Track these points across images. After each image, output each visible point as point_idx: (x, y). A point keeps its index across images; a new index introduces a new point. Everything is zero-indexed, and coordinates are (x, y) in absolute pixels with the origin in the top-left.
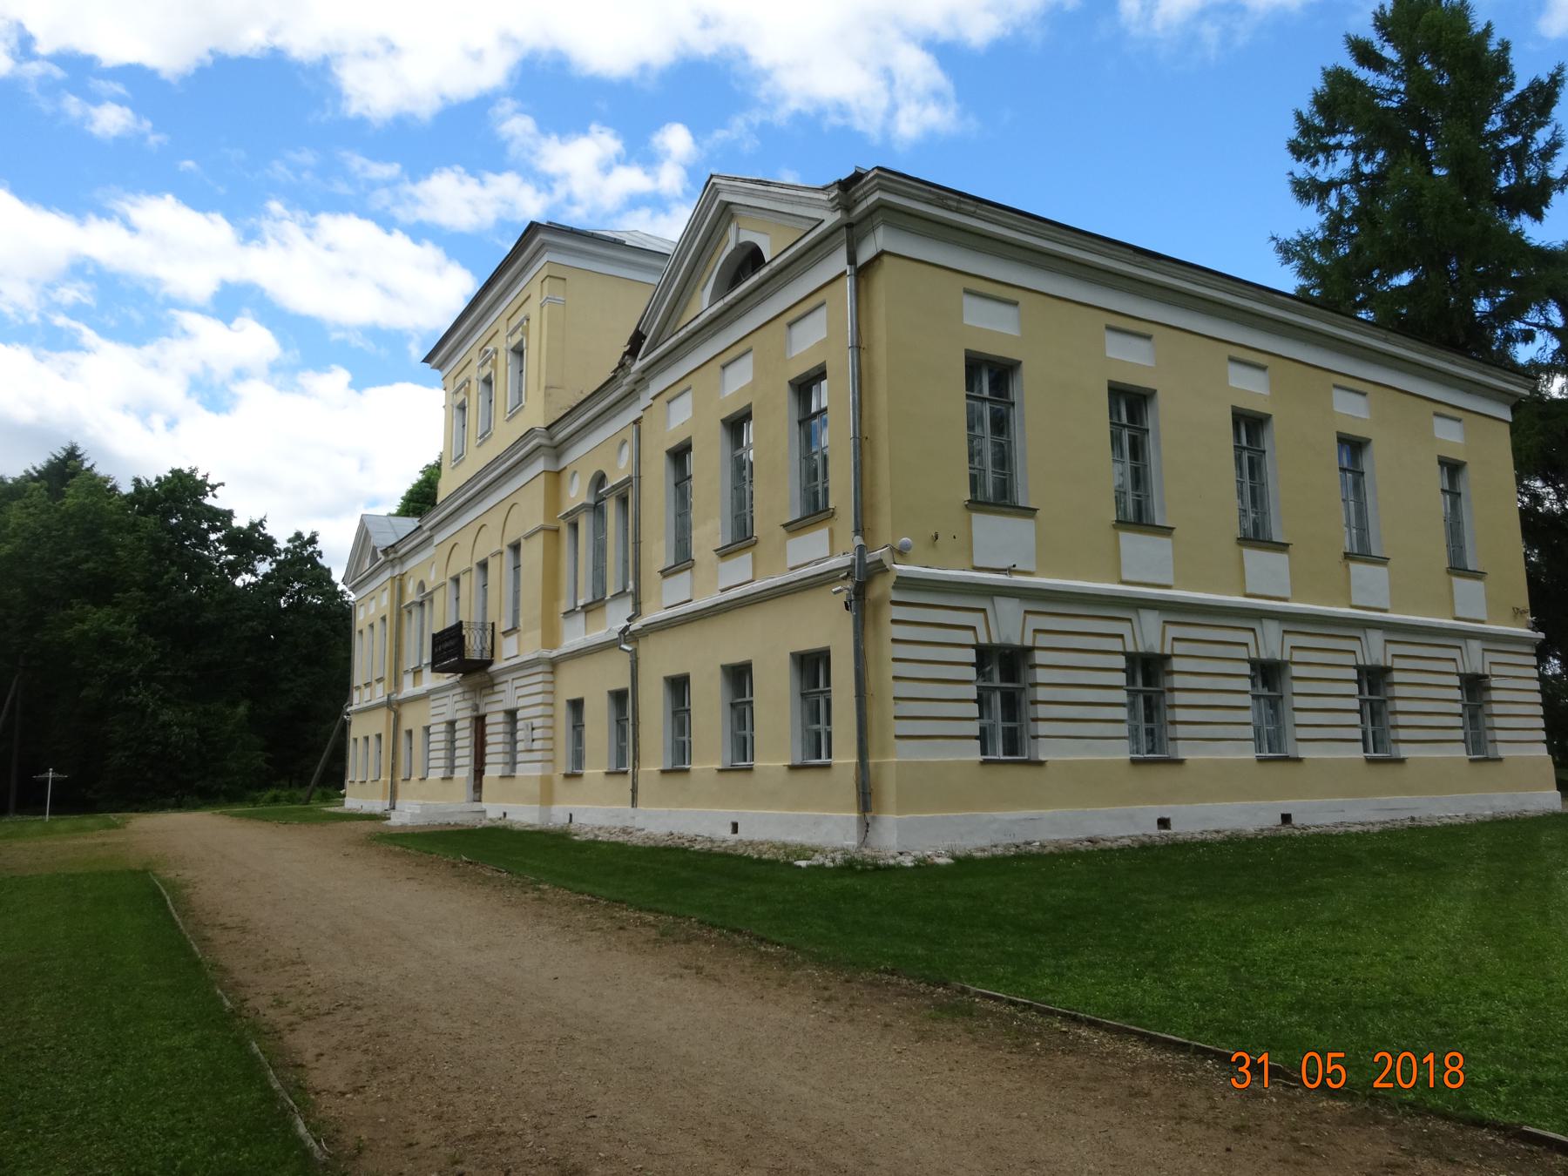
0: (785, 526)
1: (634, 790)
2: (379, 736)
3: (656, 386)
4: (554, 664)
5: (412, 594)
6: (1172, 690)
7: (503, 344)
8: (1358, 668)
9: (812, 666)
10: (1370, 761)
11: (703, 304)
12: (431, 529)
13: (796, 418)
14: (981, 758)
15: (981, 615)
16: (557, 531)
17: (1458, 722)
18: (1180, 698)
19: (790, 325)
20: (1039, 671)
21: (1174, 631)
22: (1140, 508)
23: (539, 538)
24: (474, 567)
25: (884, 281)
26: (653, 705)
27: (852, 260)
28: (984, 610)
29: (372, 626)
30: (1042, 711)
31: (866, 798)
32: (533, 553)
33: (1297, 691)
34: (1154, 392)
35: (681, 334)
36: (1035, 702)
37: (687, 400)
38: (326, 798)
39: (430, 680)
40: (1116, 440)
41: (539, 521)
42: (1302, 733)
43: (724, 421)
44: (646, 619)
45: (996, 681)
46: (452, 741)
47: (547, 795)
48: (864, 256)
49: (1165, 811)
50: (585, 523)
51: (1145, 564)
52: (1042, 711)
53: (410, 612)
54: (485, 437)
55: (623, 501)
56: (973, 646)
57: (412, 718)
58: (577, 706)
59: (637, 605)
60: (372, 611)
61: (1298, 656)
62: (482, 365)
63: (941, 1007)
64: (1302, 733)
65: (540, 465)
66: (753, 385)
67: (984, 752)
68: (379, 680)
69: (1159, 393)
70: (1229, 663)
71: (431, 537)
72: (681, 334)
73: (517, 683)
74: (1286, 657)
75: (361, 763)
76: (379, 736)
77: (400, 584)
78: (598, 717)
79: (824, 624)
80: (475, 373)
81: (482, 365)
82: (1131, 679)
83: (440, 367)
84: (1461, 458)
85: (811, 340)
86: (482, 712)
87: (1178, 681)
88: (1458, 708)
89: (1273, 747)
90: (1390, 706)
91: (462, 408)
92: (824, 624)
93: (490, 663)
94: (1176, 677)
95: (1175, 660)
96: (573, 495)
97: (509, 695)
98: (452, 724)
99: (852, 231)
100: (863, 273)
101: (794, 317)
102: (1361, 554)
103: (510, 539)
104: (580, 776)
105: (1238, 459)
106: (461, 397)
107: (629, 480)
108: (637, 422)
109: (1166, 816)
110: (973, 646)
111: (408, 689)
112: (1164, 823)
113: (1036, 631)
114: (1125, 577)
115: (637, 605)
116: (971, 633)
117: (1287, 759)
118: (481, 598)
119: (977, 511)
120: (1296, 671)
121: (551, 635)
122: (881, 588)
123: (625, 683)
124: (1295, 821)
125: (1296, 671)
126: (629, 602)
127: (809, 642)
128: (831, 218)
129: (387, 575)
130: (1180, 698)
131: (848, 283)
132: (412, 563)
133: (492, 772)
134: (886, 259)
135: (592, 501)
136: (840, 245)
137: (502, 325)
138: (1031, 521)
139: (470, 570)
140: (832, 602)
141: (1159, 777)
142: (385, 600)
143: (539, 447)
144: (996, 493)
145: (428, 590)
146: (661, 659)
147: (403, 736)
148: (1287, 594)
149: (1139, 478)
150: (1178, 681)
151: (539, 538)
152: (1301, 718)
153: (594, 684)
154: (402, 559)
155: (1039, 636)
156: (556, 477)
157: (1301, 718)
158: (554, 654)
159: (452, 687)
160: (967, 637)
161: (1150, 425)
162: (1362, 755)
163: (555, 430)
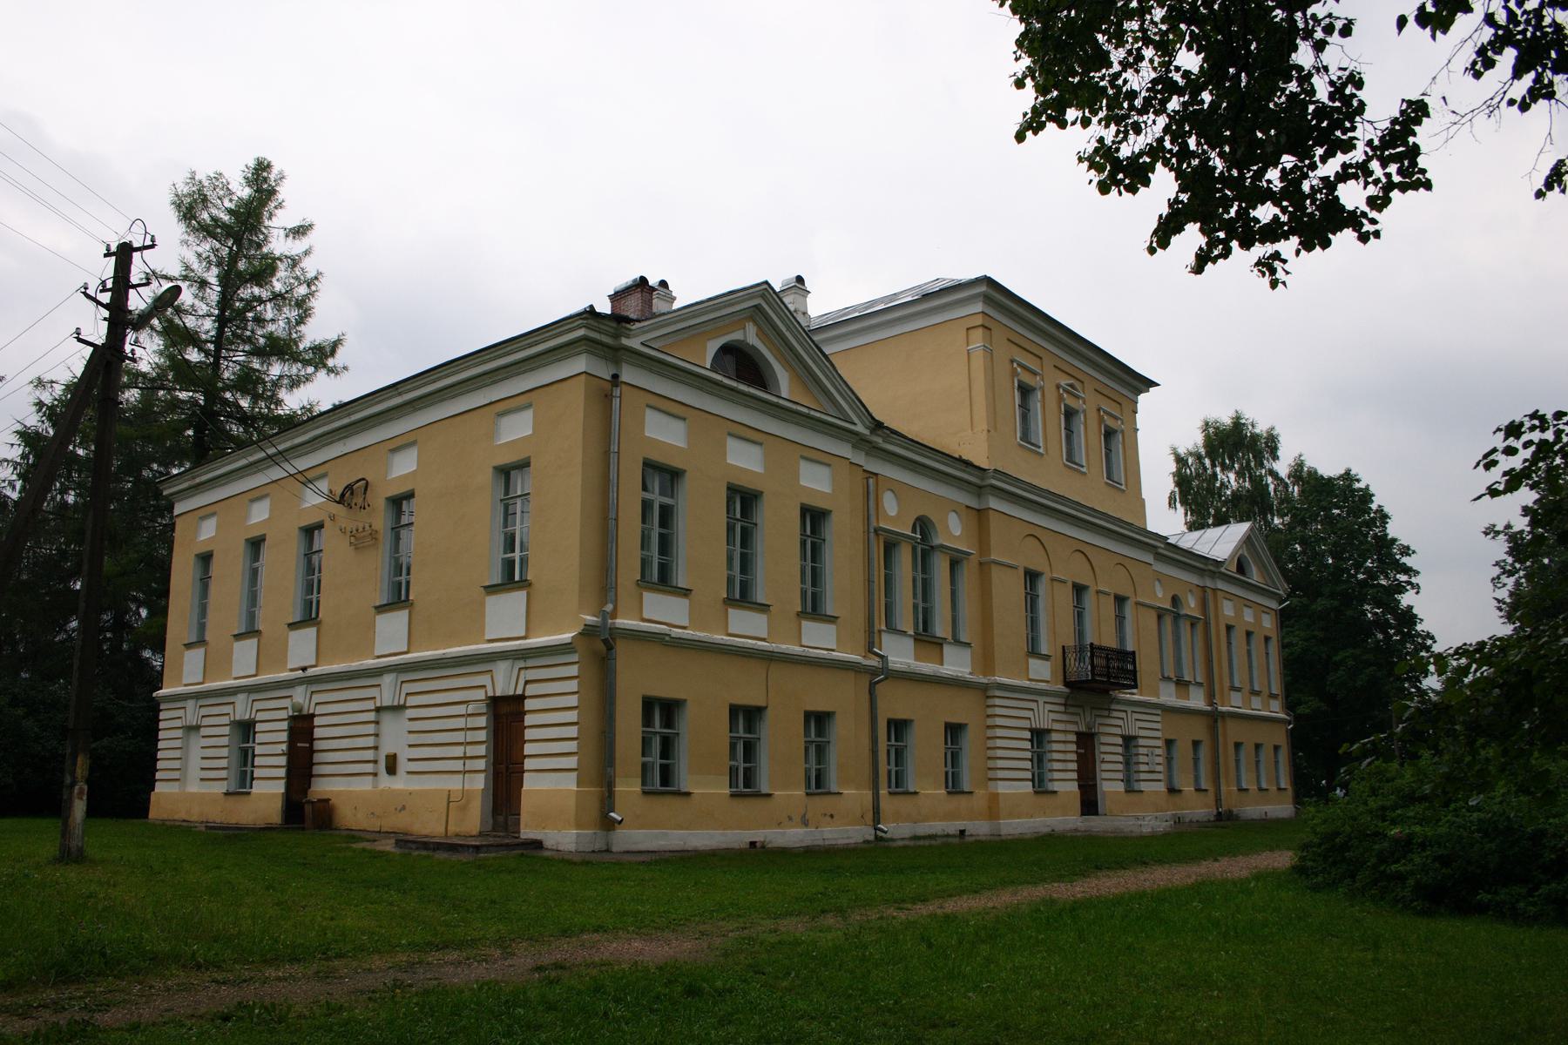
8: (1031, 730)
17: (1120, 767)
22: (746, 588)
34: (684, 471)
40: (730, 529)
45: (741, 733)
63: (1337, 834)
67: (644, 784)
69: (765, 498)
84: (677, 463)
88: (1028, 755)
89: (745, 783)
90: (1049, 756)
95: (527, 701)
105: (803, 543)
117: (907, 793)
118: (866, 705)
119: (733, 606)
133: (628, 788)
138: (833, 627)
149: (746, 564)
160: (1026, 724)
161: (759, 521)
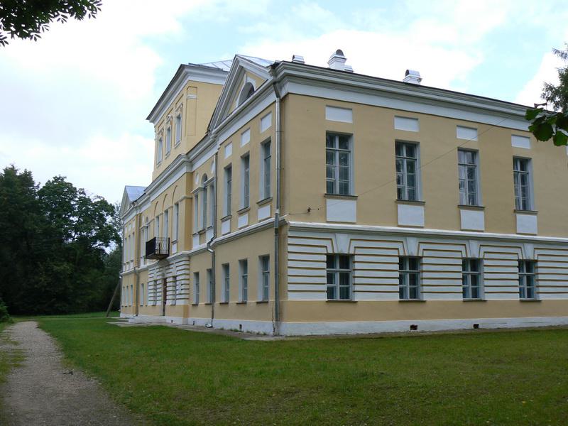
0: (258, 203)
1: (213, 312)
2: (132, 286)
3: (222, 139)
4: (189, 257)
5: (144, 224)
6: (423, 271)
7: (174, 114)
9: (265, 259)
10: (521, 301)
11: (236, 106)
12: (149, 194)
13: (264, 158)
14: (327, 300)
15: (330, 241)
16: (192, 198)
18: (425, 275)
19: (262, 119)
20: (356, 264)
21: (423, 246)
23: (184, 201)
24: (174, 205)
25: (291, 101)
26: (219, 272)
27: (278, 96)
28: (331, 239)
29: (129, 236)
30: (357, 280)
31: (278, 316)
32: (183, 206)
33: (486, 273)
35: (230, 117)
36: (355, 277)
37: (248, 133)
38: (115, 313)
39: (150, 263)
41: (184, 195)
42: (487, 289)
43: (241, 157)
44: (219, 238)
46: (213, 283)
47: (186, 313)
48: (283, 95)
49: (414, 322)
50: (201, 195)
51: (410, 217)
52: (357, 280)
53: (197, 196)
54: (168, 155)
55: (212, 187)
56: (325, 254)
57: (144, 278)
58: (197, 274)
59: (215, 233)
60: (130, 230)
61: (487, 256)
62: (177, 111)
64: (487, 289)
65: (184, 170)
66: (249, 144)
68: (132, 261)
70: (305, 270)
71: (149, 198)
72: (231, 115)
73: (177, 265)
74: (481, 257)
75: (127, 299)
76: (132, 286)
77: (139, 216)
78: (204, 277)
79: (266, 245)
80: (165, 126)
81: (177, 111)
82: (401, 268)
83: (153, 122)
85: (268, 126)
86: (165, 277)
87: (425, 268)
91: (160, 140)
92: (266, 245)
93: (168, 255)
94: (424, 266)
96: (197, 183)
97: (174, 270)
98: (155, 281)
99: (276, 85)
100: (283, 100)
101: (261, 116)
102: (525, 208)
103: (175, 201)
104: (267, 302)
106: (160, 136)
107: (212, 179)
108: (217, 154)
109: (415, 325)
110: (325, 254)
111: (143, 266)
112: (414, 327)
113: (355, 247)
114: (400, 224)
115: (215, 233)
116: (325, 249)
117: (481, 301)
120: (486, 262)
121: (189, 244)
122: (285, 231)
123: (210, 267)
124: (480, 327)
125: (486, 262)
126: (212, 231)
127: (264, 253)
128: (271, 79)
129: (134, 214)
130: (425, 275)
131: (277, 105)
132: (144, 208)
134: (290, 96)
135: (203, 187)
136: (271, 92)
137: (174, 106)
139: (162, 214)
140: (270, 237)
141: (417, 307)
142: (134, 225)
143: (184, 162)
144: (339, 189)
145: (149, 220)
146: (224, 255)
147: (141, 286)
148: (483, 229)
150: (425, 268)
151: (184, 201)
152: (487, 283)
153: (202, 265)
154: (140, 207)
155: (357, 249)
156: (191, 175)
157: (487, 283)
158: (188, 252)
159: (155, 265)
162: (398, 299)
163: (190, 154)
